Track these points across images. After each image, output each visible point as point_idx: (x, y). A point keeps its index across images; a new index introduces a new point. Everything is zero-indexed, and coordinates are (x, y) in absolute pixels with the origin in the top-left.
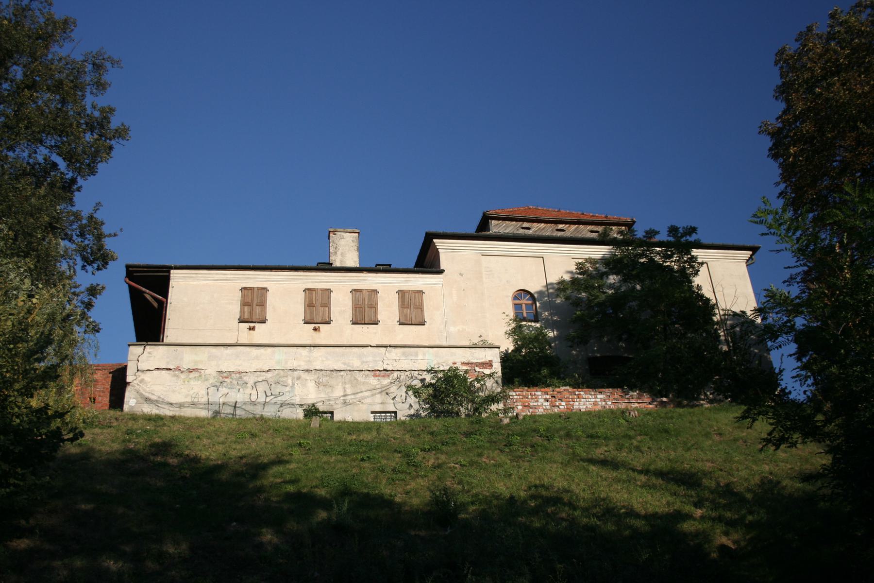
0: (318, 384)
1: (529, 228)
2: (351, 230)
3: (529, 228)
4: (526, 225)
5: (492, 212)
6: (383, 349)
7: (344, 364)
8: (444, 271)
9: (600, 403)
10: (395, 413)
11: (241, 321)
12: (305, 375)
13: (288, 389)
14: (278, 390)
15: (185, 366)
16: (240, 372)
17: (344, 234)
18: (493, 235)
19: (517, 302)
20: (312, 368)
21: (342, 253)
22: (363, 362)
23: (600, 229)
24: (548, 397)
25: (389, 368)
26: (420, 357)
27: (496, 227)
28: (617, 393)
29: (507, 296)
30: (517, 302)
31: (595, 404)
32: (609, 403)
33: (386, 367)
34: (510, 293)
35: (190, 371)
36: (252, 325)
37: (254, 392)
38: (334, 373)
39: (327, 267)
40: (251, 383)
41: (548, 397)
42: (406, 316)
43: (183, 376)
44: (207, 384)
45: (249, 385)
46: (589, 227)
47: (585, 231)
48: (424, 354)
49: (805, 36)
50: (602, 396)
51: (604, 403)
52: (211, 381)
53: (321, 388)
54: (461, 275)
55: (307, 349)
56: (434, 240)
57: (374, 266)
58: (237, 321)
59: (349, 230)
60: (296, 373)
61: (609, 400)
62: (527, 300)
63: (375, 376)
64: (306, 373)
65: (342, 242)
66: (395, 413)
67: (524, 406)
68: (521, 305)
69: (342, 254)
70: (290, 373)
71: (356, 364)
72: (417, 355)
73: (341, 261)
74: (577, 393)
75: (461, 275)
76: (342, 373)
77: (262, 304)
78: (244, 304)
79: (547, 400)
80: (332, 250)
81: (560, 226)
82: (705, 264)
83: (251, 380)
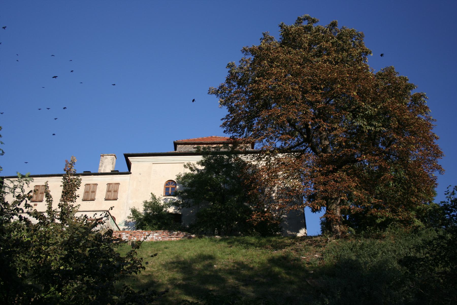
2: (111, 154)
5: (180, 140)
9: (155, 238)
17: (108, 156)
18: (178, 153)
19: (167, 186)
21: (105, 166)
23: (196, 146)
27: (180, 148)
28: (166, 233)
30: (167, 186)
31: (152, 238)
32: (160, 238)
34: (164, 183)
36: (35, 203)
39: (116, 172)
41: (128, 235)
42: (109, 196)
47: (190, 148)
50: (156, 234)
51: (157, 238)
54: (140, 174)
56: (129, 158)
57: (83, 172)
58: (82, 200)
59: (110, 154)
61: (160, 236)
62: (173, 185)
65: (106, 160)
68: (169, 188)
69: (105, 167)
73: (104, 170)
74: (144, 233)
75: (140, 174)
77: (116, 191)
78: (108, 191)
80: (100, 164)
82: (127, 170)
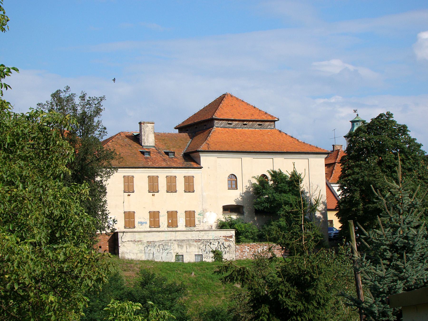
0: (178, 245)
1: (231, 124)
3: (231, 124)
4: (230, 122)
6: (198, 232)
7: (186, 238)
8: (203, 167)
10: (202, 255)
11: (125, 192)
12: (174, 242)
13: (169, 247)
14: (166, 248)
15: (137, 240)
16: (154, 241)
20: (176, 239)
22: (192, 237)
24: (249, 248)
25: (200, 239)
26: (210, 234)
29: (226, 178)
33: (199, 238)
35: (138, 241)
37: (159, 249)
38: (183, 241)
40: (157, 245)
41: (249, 248)
43: (136, 243)
44: (144, 246)
45: (157, 246)
46: (258, 123)
48: (211, 234)
49: (396, 122)
52: (145, 245)
53: (179, 246)
54: (209, 168)
55: (174, 232)
60: (171, 241)
63: (196, 242)
64: (174, 241)
66: (202, 255)
67: (241, 251)
70: (169, 241)
71: (190, 238)
72: (209, 233)
75: (209, 168)
76: (186, 241)
79: (248, 249)
81: (245, 123)
83: (157, 244)
